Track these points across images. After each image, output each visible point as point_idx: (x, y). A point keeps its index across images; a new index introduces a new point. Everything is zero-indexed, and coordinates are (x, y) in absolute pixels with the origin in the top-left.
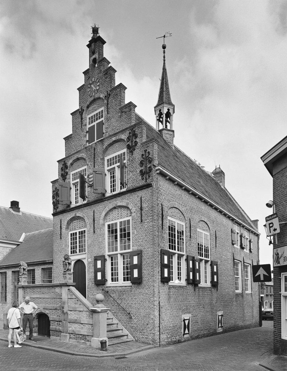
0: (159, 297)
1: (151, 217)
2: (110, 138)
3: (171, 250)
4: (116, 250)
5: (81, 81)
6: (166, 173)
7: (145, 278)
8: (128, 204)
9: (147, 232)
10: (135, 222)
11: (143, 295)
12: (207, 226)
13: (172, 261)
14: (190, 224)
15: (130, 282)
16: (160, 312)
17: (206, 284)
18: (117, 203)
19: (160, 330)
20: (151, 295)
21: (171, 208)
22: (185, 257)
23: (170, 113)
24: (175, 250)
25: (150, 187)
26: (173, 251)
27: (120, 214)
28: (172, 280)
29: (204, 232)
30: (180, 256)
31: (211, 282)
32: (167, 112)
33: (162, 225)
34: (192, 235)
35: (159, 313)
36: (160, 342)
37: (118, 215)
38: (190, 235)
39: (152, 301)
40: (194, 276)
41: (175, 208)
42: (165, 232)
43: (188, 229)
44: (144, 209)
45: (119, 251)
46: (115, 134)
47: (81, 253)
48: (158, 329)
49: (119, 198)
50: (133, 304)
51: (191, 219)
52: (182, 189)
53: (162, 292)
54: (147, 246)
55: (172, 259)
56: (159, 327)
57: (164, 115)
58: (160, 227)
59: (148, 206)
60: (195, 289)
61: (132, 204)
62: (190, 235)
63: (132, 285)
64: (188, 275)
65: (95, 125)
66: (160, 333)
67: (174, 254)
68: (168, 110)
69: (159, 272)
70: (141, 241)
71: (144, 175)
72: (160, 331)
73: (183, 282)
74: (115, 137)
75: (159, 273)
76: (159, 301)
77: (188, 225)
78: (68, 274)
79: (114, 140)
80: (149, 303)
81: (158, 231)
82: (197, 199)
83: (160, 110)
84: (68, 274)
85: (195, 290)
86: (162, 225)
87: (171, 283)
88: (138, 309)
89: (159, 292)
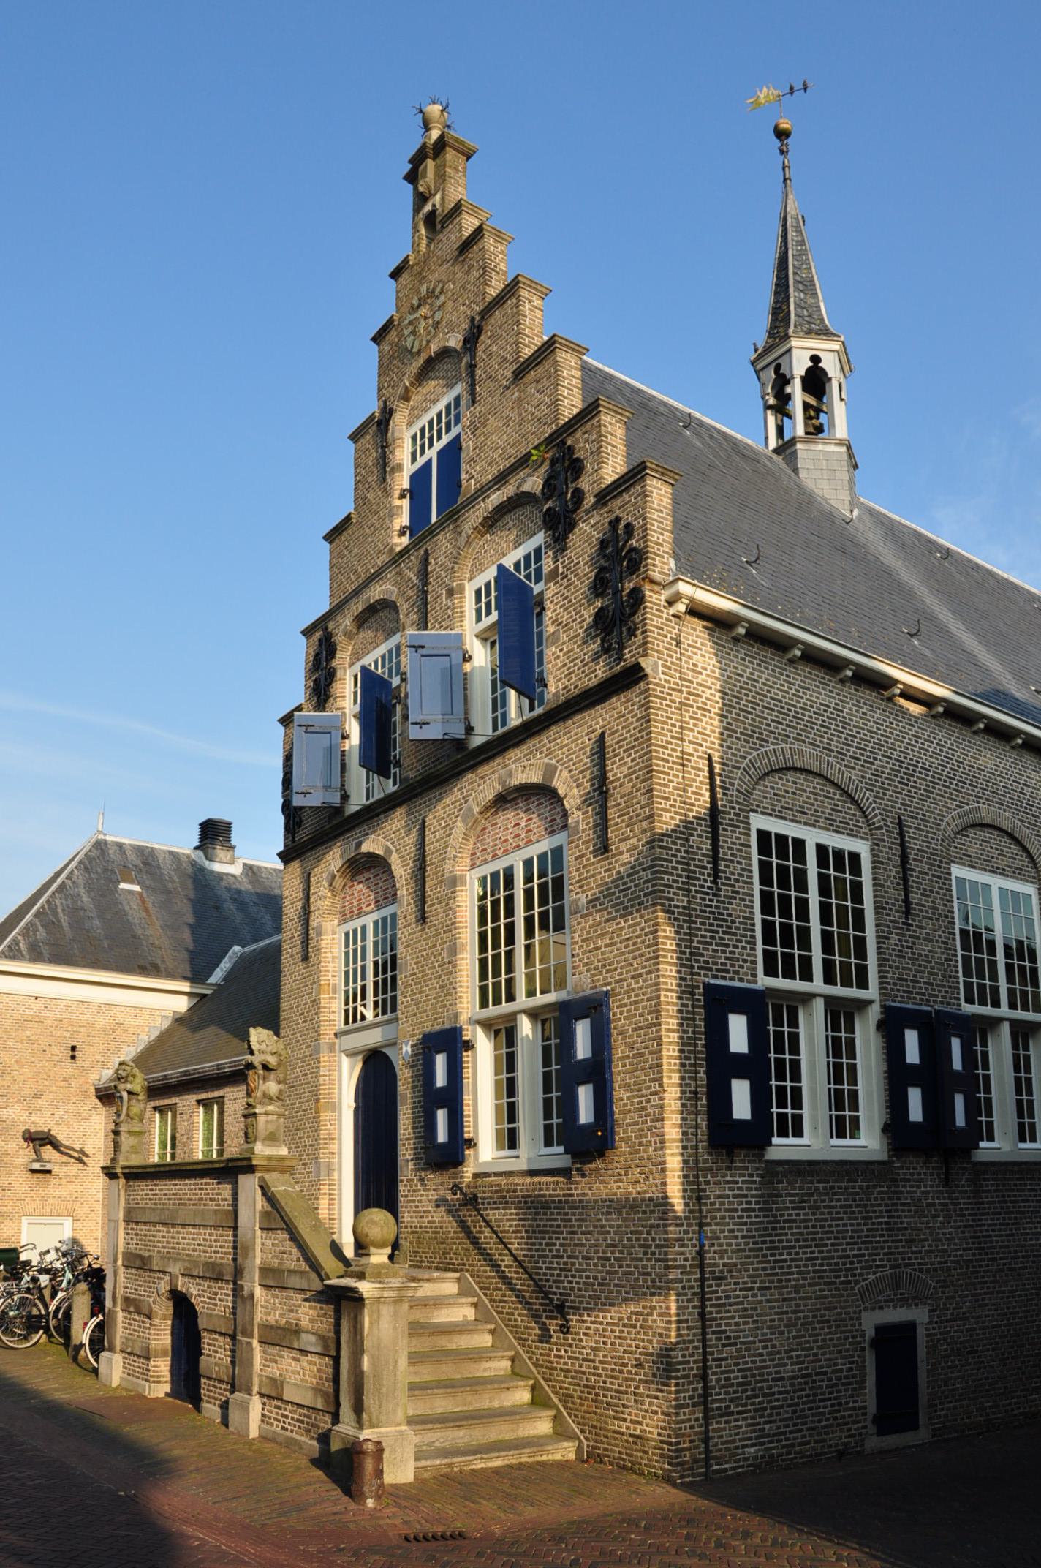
0: (701, 1225)
1: (645, 824)
2: (484, 500)
3: (975, 1009)
4: (511, 998)
5: (383, 302)
6: (969, 710)
7: (626, 1129)
8: (550, 771)
9: (629, 901)
10: (581, 857)
11: (620, 1213)
12: (1014, 849)
13: (985, 1055)
14: (903, 845)
15: (561, 1149)
16: (703, 1300)
17: (836, 1142)
18: (510, 774)
19: (705, 1395)
20: (652, 1212)
21: (772, 771)
22: (874, 1013)
23: (824, 372)
24: (807, 976)
25: (637, 682)
26: (797, 985)
27: (523, 824)
28: (991, 1139)
29: (996, 882)
30: (841, 1014)
31: (886, 1129)
32: (809, 370)
33: (715, 859)
34: (915, 898)
35: (703, 1306)
36: (707, 1459)
37: (516, 831)
38: (907, 901)
39: (657, 1246)
40: (937, 1106)
41: (984, 834)
42: (738, 893)
43: (893, 871)
44: (615, 788)
45: (522, 1000)
46: (501, 479)
47: (351, 1026)
48: (695, 1390)
49: (513, 754)
50: (577, 1258)
51: (907, 821)
52: (842, 681)
53: (719, 1197)
54: (631, 965)
55: (984, 1044)
56: (704, 1377)
57: (797, 384)
58: (705, 868)
59: (634, 773)
60: (947, 1174)
61: (565, 773)
62: (907, 901)
63: (573, 1163)
64: (896, 1104)
65: (430, 461)
66: (706, 1411)
67: (995, 1022)
68: (816, 359)
69: (696, 1093)
70: (606, 946)
71: (612, 632)
72: (705, 1403)
73: (869, 1141)
74: (498, 489)
75: (697, 1099)
76: (702, 1246)
77: (891, 854)
78: (130, 1133)
79: (496, 503)
80: (645, 1253)
81: (689, 891)
82: (850, 689)
83: (778, 367)
84: (130, 1133)
85: (947, 1181)
86: (715, 859)
87: (782, 1148)
88: (599, 1284)
89: (699, 1198)
